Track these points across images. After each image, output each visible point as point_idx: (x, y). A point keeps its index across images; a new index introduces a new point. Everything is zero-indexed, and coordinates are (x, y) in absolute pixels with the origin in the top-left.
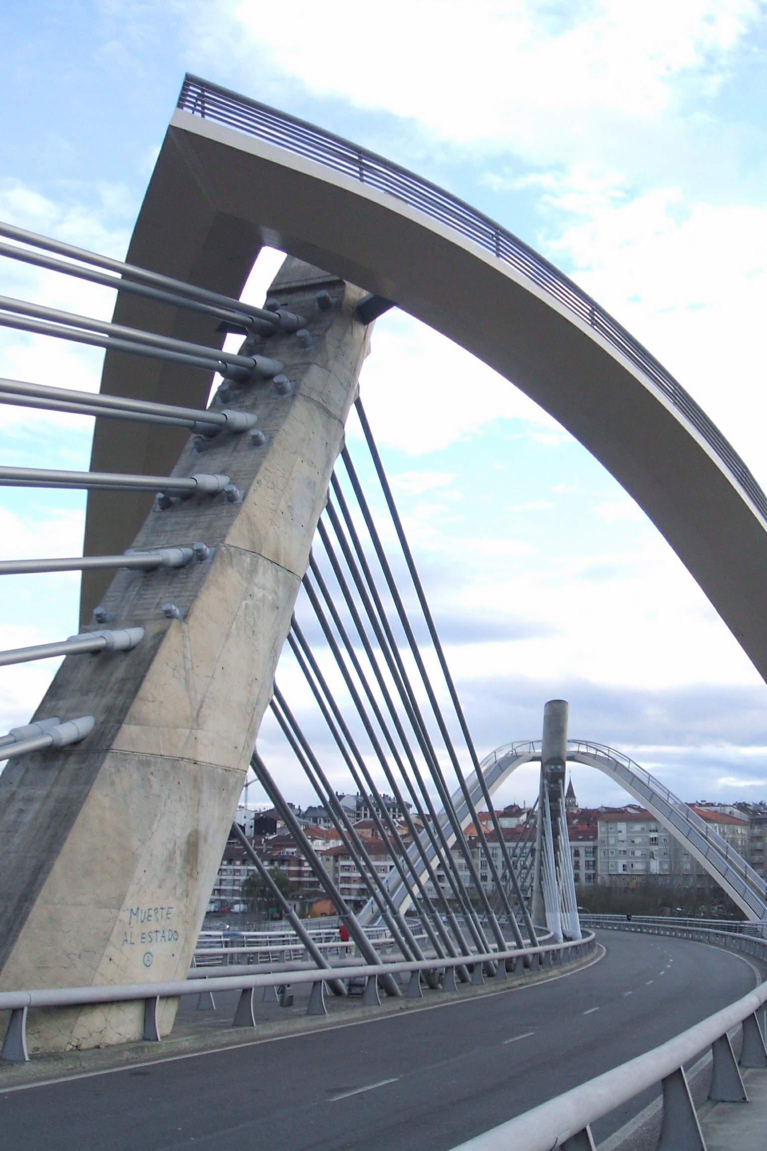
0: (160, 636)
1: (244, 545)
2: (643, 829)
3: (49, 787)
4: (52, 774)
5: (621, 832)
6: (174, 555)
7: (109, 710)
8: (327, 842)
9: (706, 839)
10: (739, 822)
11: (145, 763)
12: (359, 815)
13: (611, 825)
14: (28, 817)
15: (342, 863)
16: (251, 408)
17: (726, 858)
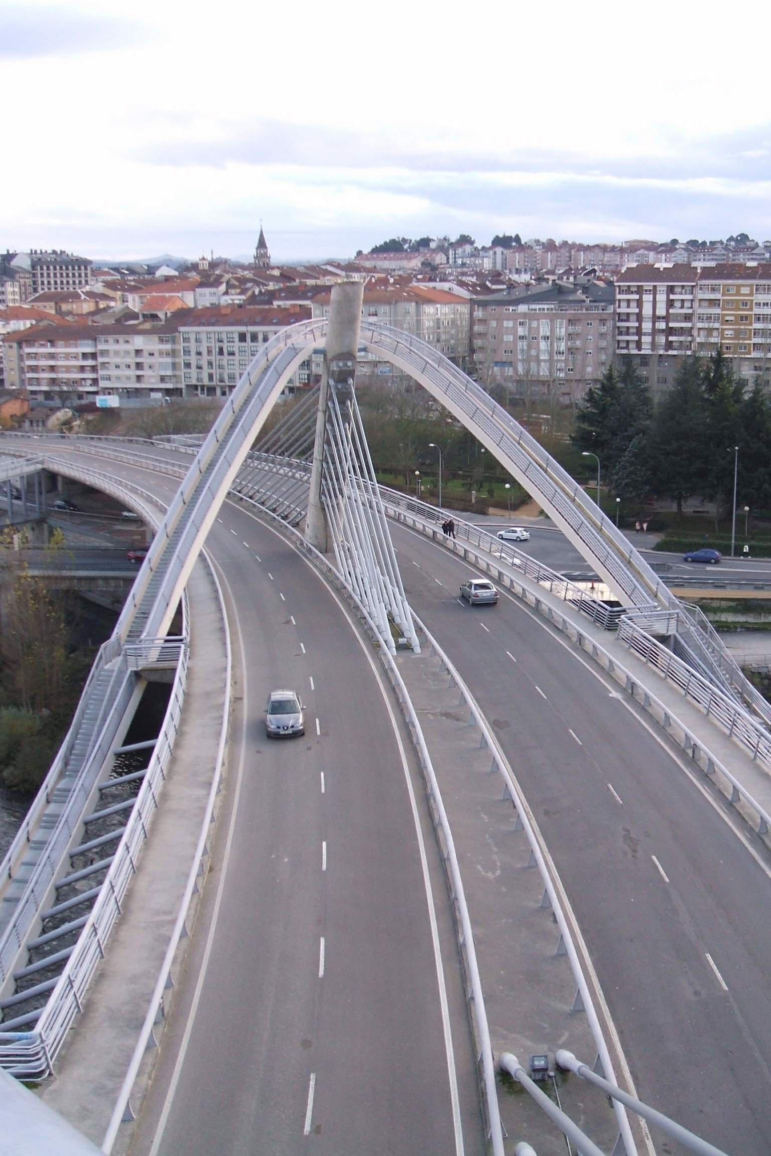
8: (8, 323)
9: (546, 471)
15: (28, 350)
17: (574, 501)
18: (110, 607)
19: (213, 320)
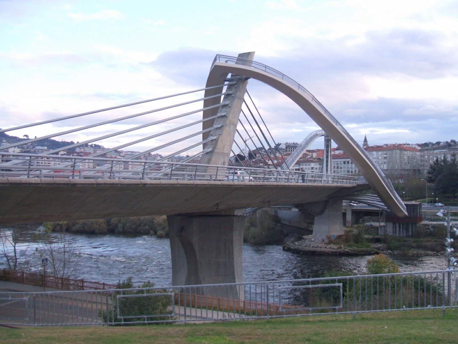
0: (219, 137)
1: (228, 123)
2: (382, 154)
3: (207, 157)
4: (208, 155)
5: (374, 155)
6: (220, 126)
7: (213, 147)
10: (417, 151)
11: (218, 153)
12: (287, 151)
13: (370, 153)
14: (206, 160)
16: (229, 100)
18: (288, 224)
19: (336, 157)
